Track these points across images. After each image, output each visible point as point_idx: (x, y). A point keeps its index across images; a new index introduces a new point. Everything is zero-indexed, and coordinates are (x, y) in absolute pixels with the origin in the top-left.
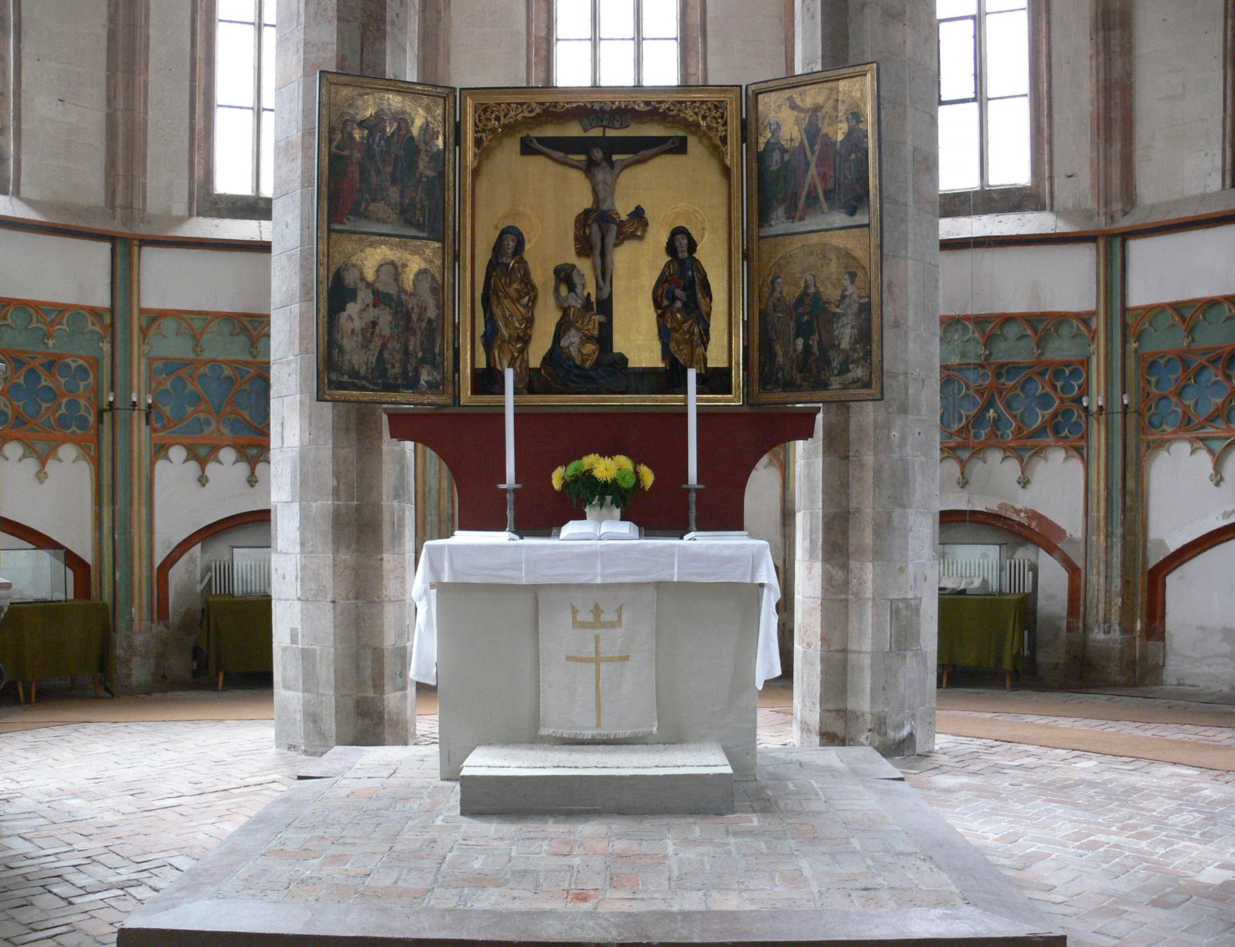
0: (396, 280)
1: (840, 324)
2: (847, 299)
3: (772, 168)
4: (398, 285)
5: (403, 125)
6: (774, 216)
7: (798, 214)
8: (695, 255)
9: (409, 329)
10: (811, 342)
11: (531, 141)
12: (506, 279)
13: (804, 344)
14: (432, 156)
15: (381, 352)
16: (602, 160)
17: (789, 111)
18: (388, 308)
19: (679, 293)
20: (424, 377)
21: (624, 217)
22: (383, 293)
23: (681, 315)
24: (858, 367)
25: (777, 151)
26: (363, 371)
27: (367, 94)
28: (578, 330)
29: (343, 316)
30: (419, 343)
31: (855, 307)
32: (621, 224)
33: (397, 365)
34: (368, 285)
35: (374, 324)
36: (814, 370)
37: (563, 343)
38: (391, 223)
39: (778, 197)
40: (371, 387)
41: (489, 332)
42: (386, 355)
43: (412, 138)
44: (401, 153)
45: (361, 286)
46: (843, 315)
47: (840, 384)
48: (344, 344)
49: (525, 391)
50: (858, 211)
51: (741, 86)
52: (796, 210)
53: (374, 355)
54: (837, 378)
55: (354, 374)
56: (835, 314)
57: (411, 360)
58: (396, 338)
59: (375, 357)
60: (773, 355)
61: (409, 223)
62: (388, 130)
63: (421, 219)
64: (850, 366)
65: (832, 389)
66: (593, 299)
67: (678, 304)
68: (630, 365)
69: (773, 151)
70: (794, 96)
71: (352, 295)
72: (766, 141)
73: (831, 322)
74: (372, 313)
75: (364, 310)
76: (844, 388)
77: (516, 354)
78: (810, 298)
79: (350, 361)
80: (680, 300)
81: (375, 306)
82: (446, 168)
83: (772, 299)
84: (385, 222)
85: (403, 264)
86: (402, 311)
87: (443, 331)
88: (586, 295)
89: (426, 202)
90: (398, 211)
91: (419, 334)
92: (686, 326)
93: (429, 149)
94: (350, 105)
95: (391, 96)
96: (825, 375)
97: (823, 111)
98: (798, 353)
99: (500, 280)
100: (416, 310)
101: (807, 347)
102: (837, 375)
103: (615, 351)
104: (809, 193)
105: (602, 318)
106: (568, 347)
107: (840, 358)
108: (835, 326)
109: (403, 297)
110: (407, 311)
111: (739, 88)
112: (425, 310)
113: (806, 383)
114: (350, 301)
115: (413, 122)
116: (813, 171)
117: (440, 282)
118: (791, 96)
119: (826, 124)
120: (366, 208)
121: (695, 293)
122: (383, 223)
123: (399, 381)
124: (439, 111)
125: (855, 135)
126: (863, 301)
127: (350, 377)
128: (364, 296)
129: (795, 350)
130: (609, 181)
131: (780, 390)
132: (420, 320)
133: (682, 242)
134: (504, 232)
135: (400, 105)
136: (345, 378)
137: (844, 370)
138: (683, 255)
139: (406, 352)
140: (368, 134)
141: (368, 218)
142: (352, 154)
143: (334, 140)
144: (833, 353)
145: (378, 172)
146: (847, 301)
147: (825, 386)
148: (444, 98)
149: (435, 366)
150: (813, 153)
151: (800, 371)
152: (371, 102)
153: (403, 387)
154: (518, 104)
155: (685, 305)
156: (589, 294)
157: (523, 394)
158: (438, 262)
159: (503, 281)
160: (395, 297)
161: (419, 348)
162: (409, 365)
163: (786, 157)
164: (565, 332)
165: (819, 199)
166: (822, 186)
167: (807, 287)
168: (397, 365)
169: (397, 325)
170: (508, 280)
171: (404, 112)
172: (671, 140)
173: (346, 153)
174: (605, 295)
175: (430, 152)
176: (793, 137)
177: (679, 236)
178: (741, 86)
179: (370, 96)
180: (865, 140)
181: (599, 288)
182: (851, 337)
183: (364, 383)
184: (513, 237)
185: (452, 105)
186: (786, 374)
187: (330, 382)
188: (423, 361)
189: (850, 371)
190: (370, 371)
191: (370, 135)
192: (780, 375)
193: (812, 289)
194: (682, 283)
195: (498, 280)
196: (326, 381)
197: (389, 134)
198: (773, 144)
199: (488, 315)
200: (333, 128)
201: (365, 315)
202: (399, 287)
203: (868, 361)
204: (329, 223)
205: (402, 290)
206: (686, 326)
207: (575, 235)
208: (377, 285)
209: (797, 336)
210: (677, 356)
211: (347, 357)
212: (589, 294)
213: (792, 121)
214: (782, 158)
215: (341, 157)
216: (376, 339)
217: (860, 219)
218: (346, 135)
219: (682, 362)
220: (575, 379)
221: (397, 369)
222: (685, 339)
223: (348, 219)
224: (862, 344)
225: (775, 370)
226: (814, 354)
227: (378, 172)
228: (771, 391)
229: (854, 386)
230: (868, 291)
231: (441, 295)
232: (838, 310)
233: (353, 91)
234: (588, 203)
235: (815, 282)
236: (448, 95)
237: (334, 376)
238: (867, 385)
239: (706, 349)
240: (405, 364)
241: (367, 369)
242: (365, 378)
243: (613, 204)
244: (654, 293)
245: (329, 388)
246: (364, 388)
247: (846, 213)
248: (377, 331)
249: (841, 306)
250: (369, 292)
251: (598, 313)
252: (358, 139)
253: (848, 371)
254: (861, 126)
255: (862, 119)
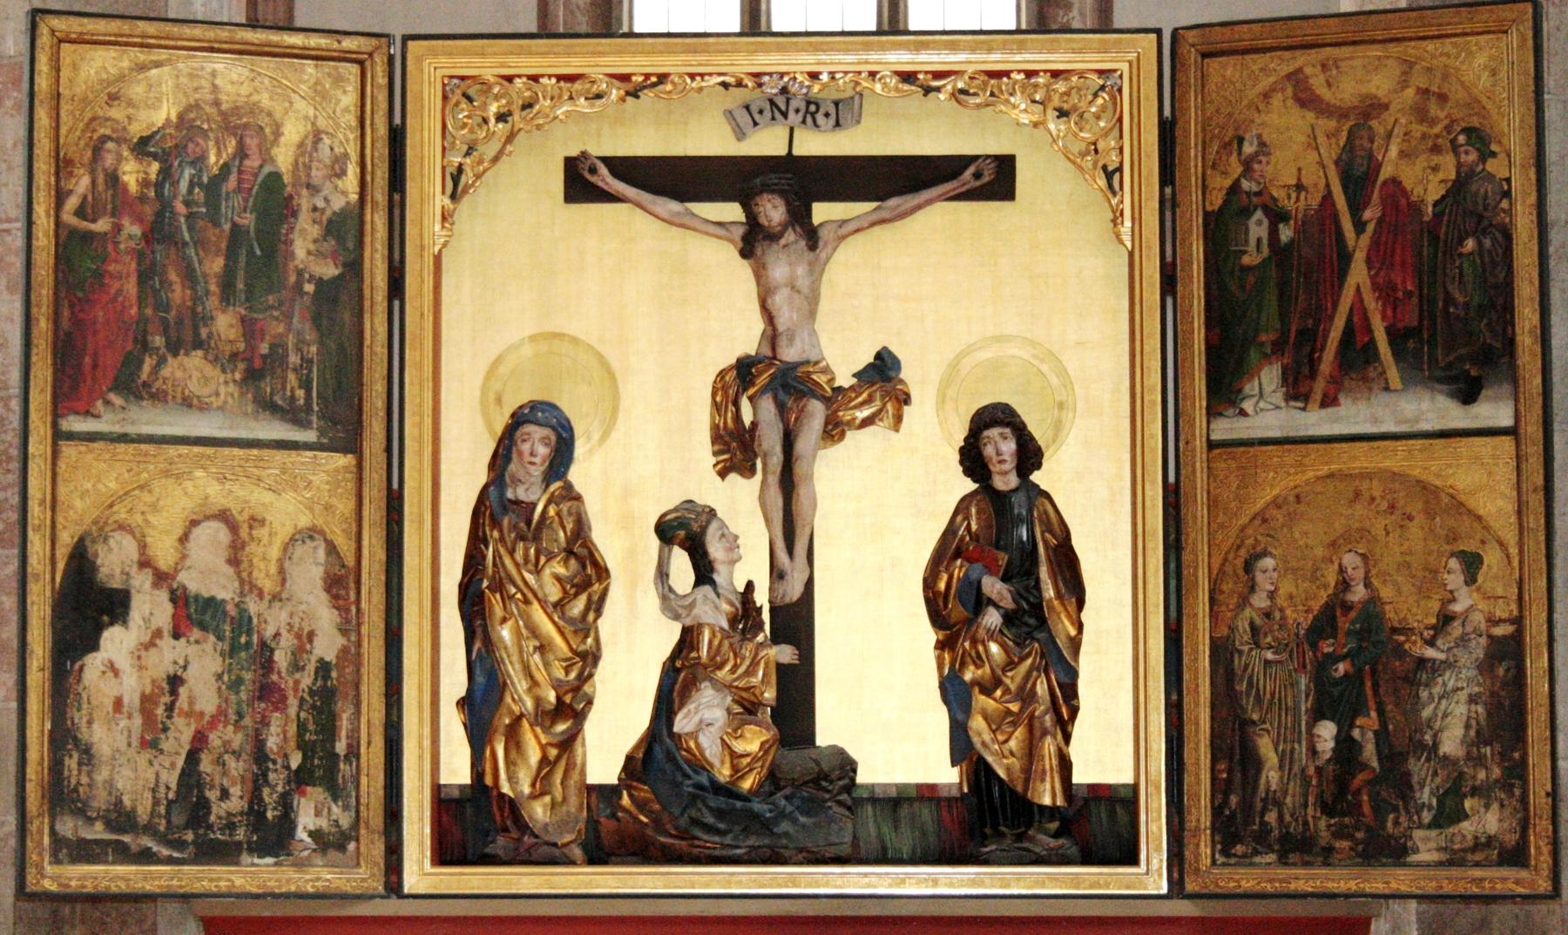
0: (234, 561)
1: (1437, 690)
2: (1456, 624)
3: (1246, 260)
4: (239, 574)
5: (251, 143)
6: (1251, 388)
7: (1319, 386)
8: (1036, 477)
9: (268, 693)
10: (1356, 733)
11: (593, 171)
12: (526, 550)
13: (1337, 739)
14: (330, 221)
15: (193, 757)
16: (785, 226)
17: (1296, 111)
18: (212, 638)
19: (993, 586)
20: (307, 819)
21: (845, 379)
22: (197, 598)
23: (1003, 646)
24: (1487, 807)
25: (1259, 214)
26: (143, 813)
27: (158, 64)
28: (721, 686)
29: (93, 664)
30: (292, 729)
31: (1479, 648)
32: (835, 398)
33: (235, 791)
34: (161, 578)
35: (175, 682)
36: (1366, 809)
37: (682, 724)
38: (221, 408)
39: (1263, 337)
40: (165, 852)
41: (478, 694)
42: (206, 765)
43: (276, 176)
44: (248, 220)
45: (141, 582)
46: (1449, 665)
47: (1439, 849)
48: (95, 739)
49: (577, 852)
50: (1484, 393)
51: (1158, 32)
52: (1313, 375)
53: (173, 765)
54: (1434, 833)
55: (120, 818)
56: (1422, 662)
57: (272, 776)
58: (233, 717)
59: (178, 771)
60: (1250, 763)
61: (269, 407)
62: (212, 159)
63: (300, 393)
64: (1468, 804)
65: (1418, 865)
66: (761, 598)
67: (992, 618)
68: (862, 778)
69: (1246, 212)
70: (1308, 70)
71: (115, 606)
72: (1228, 183)
73: (1411, 680)
74: (169, 653)
75: (150, 645)
76: (1450, 863)
77: (553, 752)
78: (1353, 614)
79: (110, 783)
80: (997, 607)
81: (176, 635)
82: (367, 253)
83: (1248, 612)
84: (201, 407)
85: (253, 518)
86: (248, 644)
87: (358, 695)
88: (741, 589)
89: (314, 349)
90: (238, 376)
91: (293, 703)
92: (1013, 680)
93: (320, 204)
94: (113, 98)
95: (219, 67)
96: (1396, 823)
97: (1389, 117)
98: (1319, 763)
99: (512, 552)
100: (286, 641)
101: (1346, 747)
102: (1429, 827)
103: (823, 739)
104: (1349, 332)
105: (785, 654)
106: (694, 735)
107: (1438, 780)
108: (1424, 694)
109: (253, 606)
110: (263, 644)
111: (1153, 36)
112: (311, 641)
113: (1345, 844)
114: (111, 624)
115: (277, 133)
116: (1359, 274)
117: (350, 561)
118: (1299, 70)
119: (1394, 151)
120: (156, 369)
121: (1037, 585)
122: (201, 409)
123: (240, 835)
124: (349, 99)
125: (1474, 188)
126: (1499, 631)
127: (110, 826)
128: (150, 607)
129: (1313, 752)
130: (803, 283)
131: (1272, 857)
132: (296, 667)
133: (1001, 446)
134: (519, 419)
135: (245, 90)
136: (98, 832)
137: (1450, 814)
138: (1006, 481)
139: (260, 756)
140: (160, 172)
141: (159, 397)
142: (118, 228)
143: (71, 191)
144: (1417, 768)
145: (189, 276)
146: (1456, 629)
147: (1396, 852)
148: (361, 63)
149: (335, 792)
150: (1360, 226)
151: (1327, 809)
152: (168, 86)
153: (251, 851)
154: (560, 78)
155: (1009, 618)
156: (750, 586)
157: (572, 863)
158: (345, 506)
159: (519, 555)
160: (232, 610)
161: (293, 744)
162: (266, 791)
163: (1286, 233)
164: (685, 697)
165: (1376, 349)
166: (1384, 317)
167: (1344, 585)
168: (235, 791)
169: (236, 685)
170: (532, 551)
171: (254, 109)
172: (971, 170)
173: (102, 225)
174: (794, 591)
175: (323, 211)
176: (1304, 181)
177: (994, 433)
178: (1158, 32)
179: (166, 69)
180: (1504, 204)
181: (777, 574)
182: (1467, 727)
183: (147, 842)
184: (546, 432)
185: (382, 80)
186: (1288, 818)
187: (58, 842)
188: (301, 779)
189: (1466, 817)
190: (162, 809)
191: (165, 173)
192: (1271, 817)
193: (1358, 594)
194: (1003, 559)
195: (502, 551)
196: (46, 840)
197: (215, 170)
198: (1248, 194)
199: (477, 645)
200: (69, 162)
201: (151, 657)
202: (242, 582)
203: (1517, 792)
204: (56, 416)
205: (248, 586)
206: (1013, 680)
207: (715, 428)
208: (183, 577)
209: (1318, 715)
210: (990, 759)
211: (102, 775)
212: (750, 586)
213: (1303, 138)
214: (1273, 233)
215: (87, 237)
216: (179, 721)
217: (1494, 411)
218: (101, 179)
219: (1002, 773)
220: (710, 820)
221: (236, 803)
222: (1009, 712)
223: (107, 403)
224: (1497, 747)
225: (1259, 805)
226: (1364, 766)
227: (189, 276)
228: (1245, 860)
229: (1478, 857)
230: (1514, 607)
231: (352, 596)
232: (1430, 653)
233: (119, 59)
234: (746, 338)
235: (1367, 573)
236: (371, 55)
237: (68, 827)
238: (1516, 856)
239: (1067, 738)
240: (258, 782)
241: (156, 803)
242: (149, 829)
243: (815, 343)
244: (929, 583)
245: (56, 861)
246: (146, 857)
247: (1452, 395)
248: (182, 701)
249: (1439, 642)
250: (163, 596)
251: (776, 638)
252: (133, 187)
253: (1461, 815)
254: (1495, 167)
255: (1494, 147)
